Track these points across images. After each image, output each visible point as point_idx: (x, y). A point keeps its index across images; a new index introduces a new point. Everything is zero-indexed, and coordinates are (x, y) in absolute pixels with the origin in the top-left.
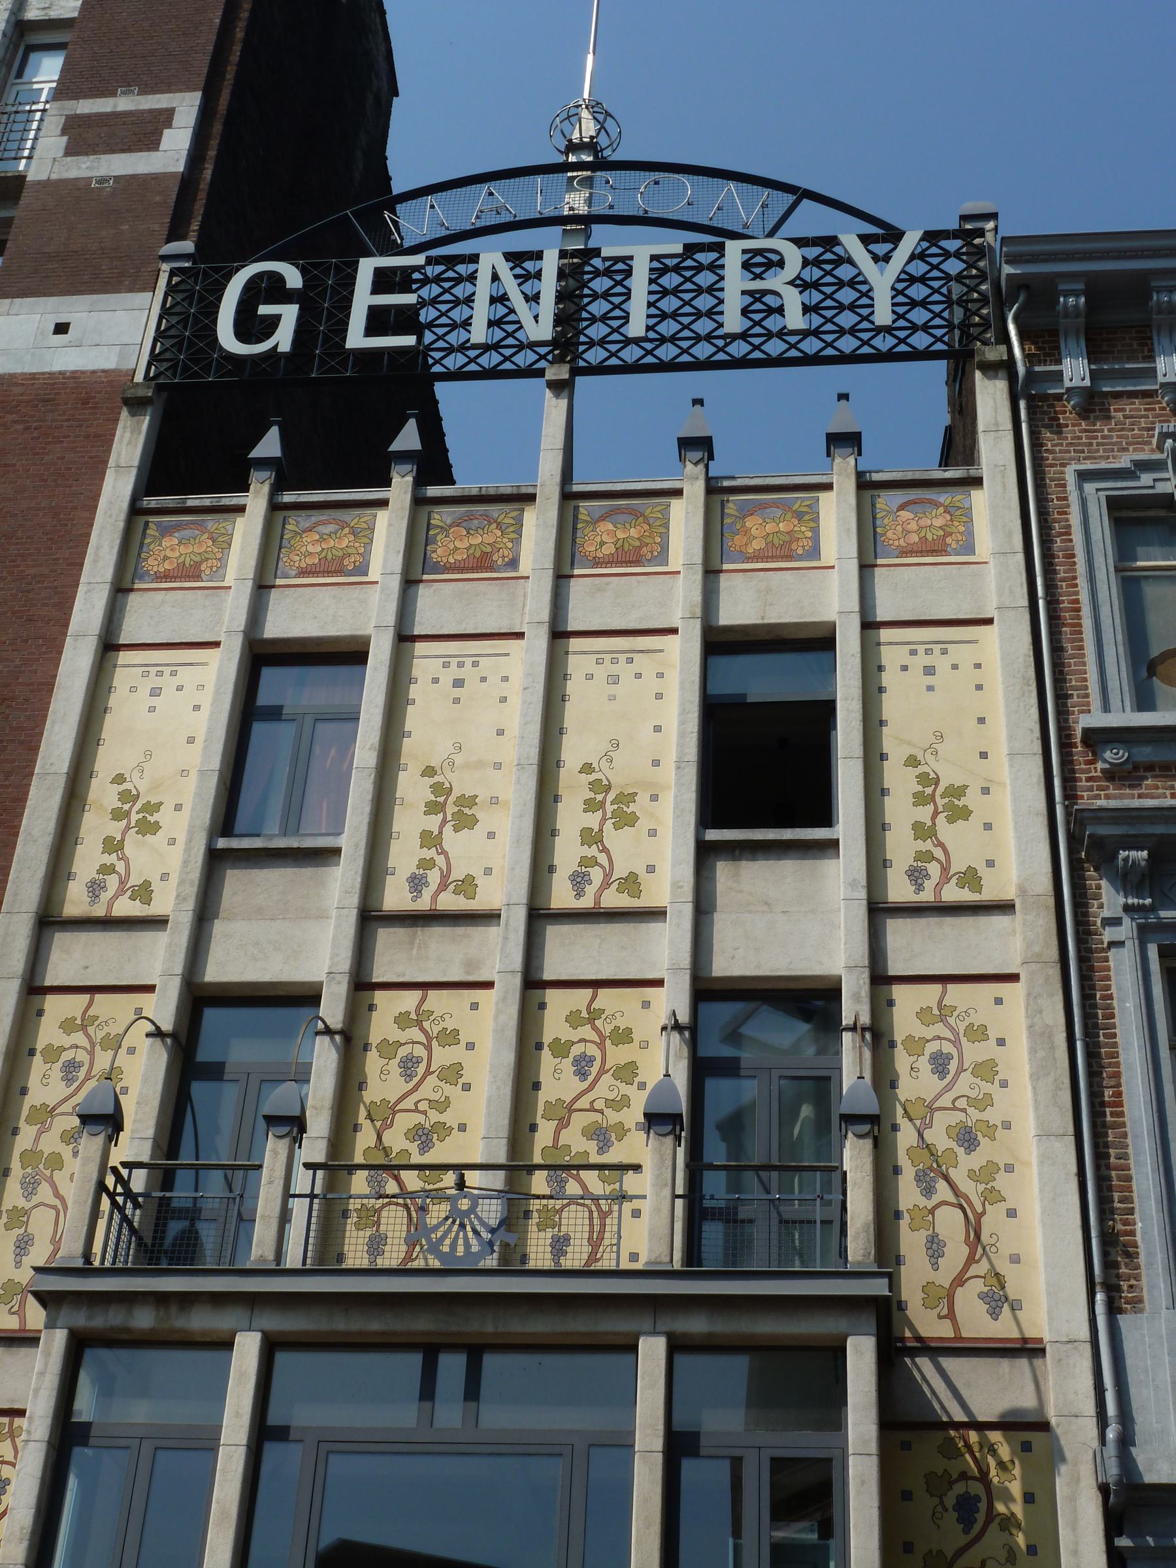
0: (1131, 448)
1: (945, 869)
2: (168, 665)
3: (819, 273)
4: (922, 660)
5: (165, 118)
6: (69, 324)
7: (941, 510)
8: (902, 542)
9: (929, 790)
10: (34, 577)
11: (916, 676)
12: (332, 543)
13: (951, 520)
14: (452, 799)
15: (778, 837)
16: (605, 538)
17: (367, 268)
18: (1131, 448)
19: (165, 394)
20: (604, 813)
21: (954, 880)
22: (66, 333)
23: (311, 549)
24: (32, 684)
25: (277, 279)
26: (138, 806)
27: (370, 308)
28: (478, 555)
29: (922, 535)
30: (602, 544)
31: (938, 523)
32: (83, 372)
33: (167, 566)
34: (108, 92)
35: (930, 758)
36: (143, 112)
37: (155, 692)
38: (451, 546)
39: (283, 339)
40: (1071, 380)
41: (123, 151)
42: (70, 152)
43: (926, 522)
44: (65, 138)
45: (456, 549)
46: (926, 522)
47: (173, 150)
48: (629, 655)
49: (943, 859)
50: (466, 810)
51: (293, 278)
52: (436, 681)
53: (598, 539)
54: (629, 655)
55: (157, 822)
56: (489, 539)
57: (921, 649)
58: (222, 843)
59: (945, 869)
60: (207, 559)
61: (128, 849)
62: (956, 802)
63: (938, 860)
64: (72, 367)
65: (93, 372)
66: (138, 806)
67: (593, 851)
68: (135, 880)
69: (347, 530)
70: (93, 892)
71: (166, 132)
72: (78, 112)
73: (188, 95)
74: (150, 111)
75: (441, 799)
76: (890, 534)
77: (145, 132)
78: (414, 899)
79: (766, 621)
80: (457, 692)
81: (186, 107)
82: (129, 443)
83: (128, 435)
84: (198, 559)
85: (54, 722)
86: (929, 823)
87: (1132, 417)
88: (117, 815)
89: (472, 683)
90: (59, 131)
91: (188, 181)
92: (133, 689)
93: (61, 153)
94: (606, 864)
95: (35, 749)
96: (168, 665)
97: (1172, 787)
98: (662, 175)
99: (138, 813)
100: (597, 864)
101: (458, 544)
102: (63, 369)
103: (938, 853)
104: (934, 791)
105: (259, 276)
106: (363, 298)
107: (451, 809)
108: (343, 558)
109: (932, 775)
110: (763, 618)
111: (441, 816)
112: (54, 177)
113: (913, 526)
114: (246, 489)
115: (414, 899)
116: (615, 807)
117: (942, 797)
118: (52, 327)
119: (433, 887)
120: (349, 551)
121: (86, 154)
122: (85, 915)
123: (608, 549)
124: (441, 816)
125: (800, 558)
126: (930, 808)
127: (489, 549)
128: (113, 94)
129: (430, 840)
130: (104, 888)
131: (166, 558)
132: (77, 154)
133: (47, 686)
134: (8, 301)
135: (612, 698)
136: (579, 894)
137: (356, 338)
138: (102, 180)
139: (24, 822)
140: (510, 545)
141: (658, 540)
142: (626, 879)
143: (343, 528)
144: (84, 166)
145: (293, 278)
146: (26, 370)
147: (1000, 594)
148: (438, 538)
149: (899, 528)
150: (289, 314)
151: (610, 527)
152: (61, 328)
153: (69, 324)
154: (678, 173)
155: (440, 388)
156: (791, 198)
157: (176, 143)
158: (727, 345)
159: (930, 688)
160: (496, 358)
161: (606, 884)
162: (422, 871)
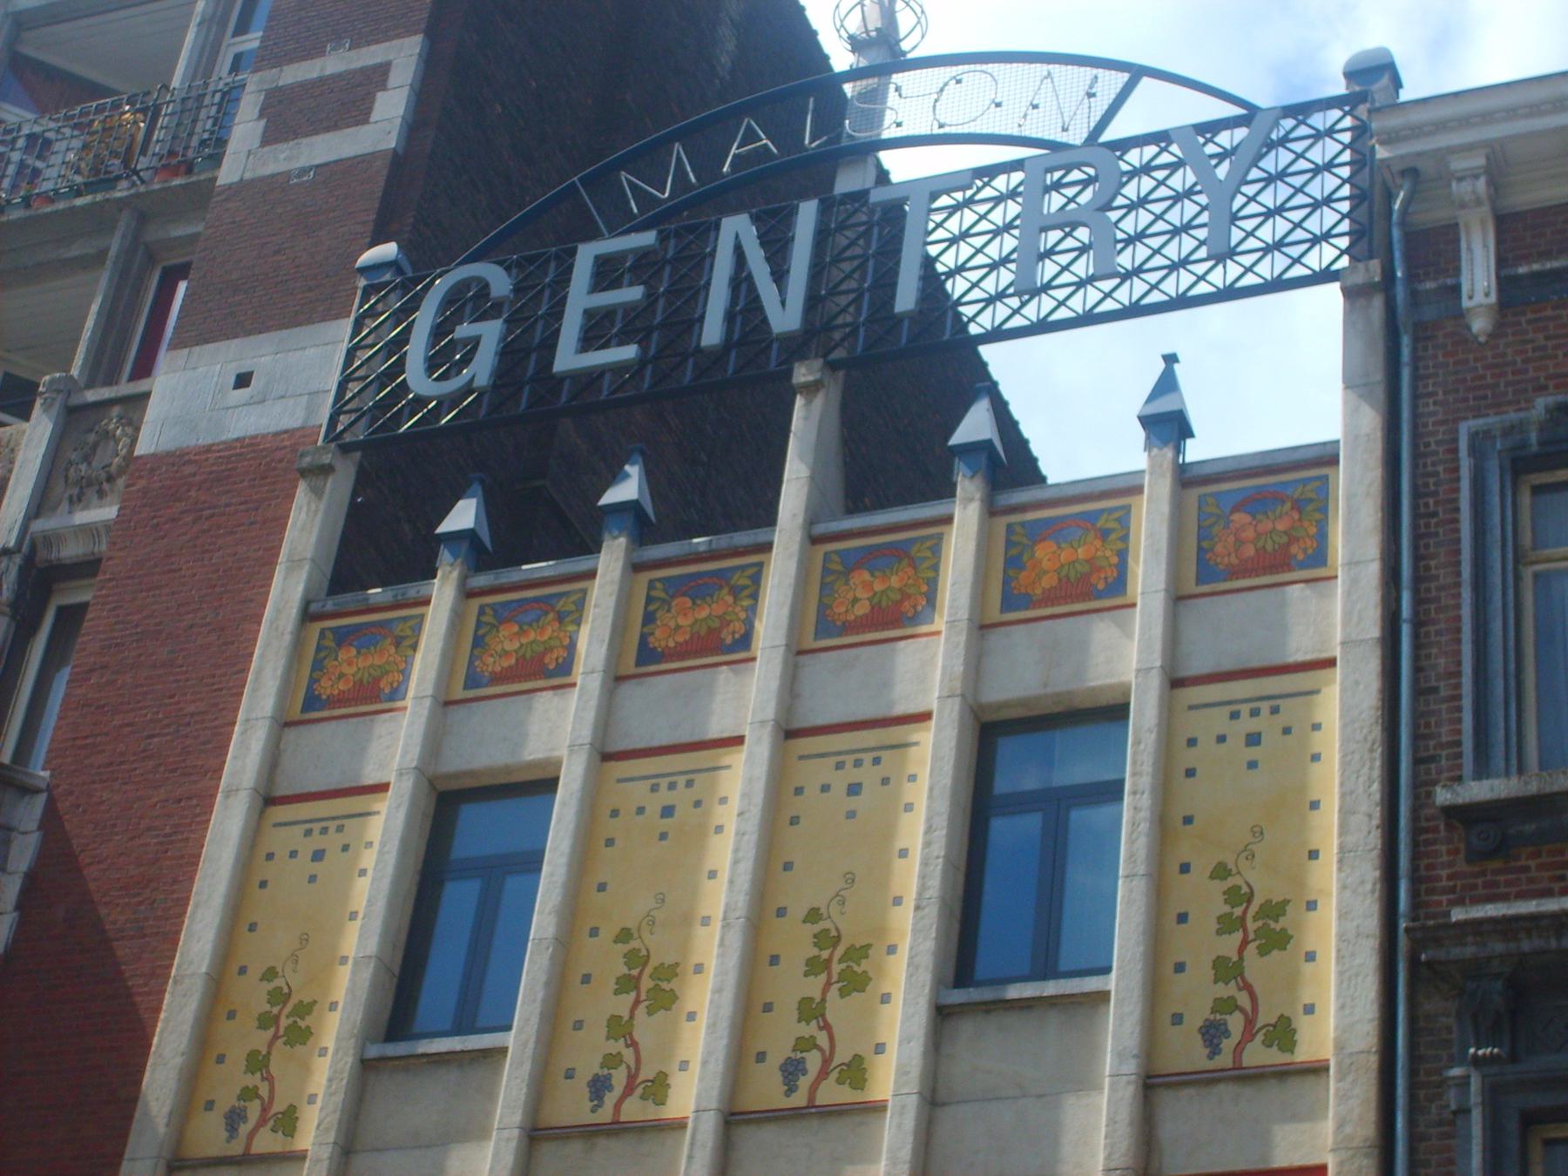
0: (1551, 384)
1: (1250, 1022)
2: (333, 818)
3: (1173, 182)
4: (1248, 724)
5: (377, 77)
6: (251, 374)
7: (1288, 505)
8: (1234, 560)
9: (1238, 911)
10: (192, 715)
11: (304, 863)
12: (532, 636)
13: (1300, 520)
14: (649, 970)
15: (1037, 993)
16: (861, 593)
17: (586, 255)
18: (1551, 384)
19: (841, 374)
20: (829, 976)
21: (1260, 1037)
22: (248, 386)
23: (508, 646)
24: (182, 857)
25: (484, 287)
26: (840, 950)
27: (588, 313)
28: (703, 632)
29: (1260, 544)
30: (855, 600)
31: (1281, 526)
32: (264, 436)
33: (342, 686)
34: (314, 51)
35: (834, 910)
36: (353, 73)
37: (854, 789)
38: (672, 624)
39: (481, 369)
40: (1471, 298)
41: (328, 129)
42: (268, 139)
43: (1266, 525)
44: (263, 123)
45: (678, 627)
46: (1266, 525)
47: (387, 121)
48: (875, 754)
49: (1248, 1007)
50: (664, 985)
51: (500, 282)
52: (641, 810)
53: (850, 596)
54: (840, 758)
55: (308, 1027)
56: (718, 609)
57: (1245, 709)
58: (957, 996)
59: (1250, 1022)
60: (387, 673)
61: (274, 1068)
62: (1273, 925)
63: (1242, 1010)
64: (251, 431)
65: (276, 434)
66: (840, 950)
67: (1230, 990)
68: (842, 1056)
69: (551, 616)
70: (1211, 1044)
71: (379, 94)
72: (281, 83)
73: (407, 41)
74: (362, 70)
75: (635, 972)
76: (1219, 548)
77: (349, 101)
78: (1211, 1056)
79: (1049, 690)
80: (1253, 753)
81: (403, 57)
82: (308, 526)
83: (303, 515)
84: (377, 673)
85: (197, 906)
86: (1235, 958)
87: (1557, 337)
88: (266, 1021)
89: (1271, 737)
90: (256, 115)
91: (398, 161)
92: (825, 788)
93: (257, 143)
94: (1248, 1006)
95: (175, 942)
96: (333, 818)
97: (1562, 878)
98: (961, 68)
99: (840, 961)
100: (1237, 1007)
101: (682, 621)
102: (242, 435)
103: (1243, 999)
104: (641, 973)
105: (464, 285)
106: (580, 298)
107: (646, 983)
108: (544, 654)
109: (1245, 889)
110: (1045, 686)
111: (633, 995)
112: (248, 176)
113: (1249, 534)
114: (951, 493)
115: (1211, 1056)
116: (1260, 923)
117: (1255, 919)
118: (232, 380)
119: (1236, 1036)
120: (553, 643)
121: (286, 140)
122: (222, 1154)
123: (862, 609)
124: (633, 995)
125: (1100, 595)
126: (1238, 936)
127: (716, 624)
128: (320, 52)
129: (1227, 970)
130: (244, 1119)
131: (341, 676)
132: (276, 141)
133: (192, 861)
134: (186, 351)
135: (851, 815)
136: (791, 1089)
137: (568, 358)
138: (304, 171)
139: (155, 1040)
140: (743, 615)
141: (924, 588)
142: (848, 1065)
143: (547, 613)
144: (282, 157)
145: (500, 282)
146: (201, 442)
147: (1345, 624)
148: (658, 615)
149: (1231, 539)
150: (490, 333)
151: (866, 576)
152: (243, 381)
153: (251, 374)
154: (987, 62)
155: (986, 351)
156: (1124, 77)
157: (391, 107)
158: (1023, 304)
159: (1252, 765)
160: (1280, 262)
161: (824, 1073)
162: (606, 1071)
